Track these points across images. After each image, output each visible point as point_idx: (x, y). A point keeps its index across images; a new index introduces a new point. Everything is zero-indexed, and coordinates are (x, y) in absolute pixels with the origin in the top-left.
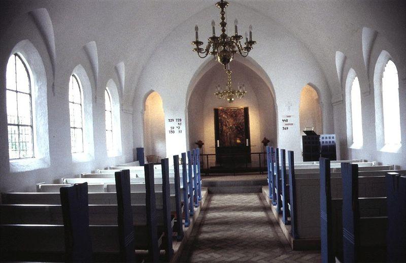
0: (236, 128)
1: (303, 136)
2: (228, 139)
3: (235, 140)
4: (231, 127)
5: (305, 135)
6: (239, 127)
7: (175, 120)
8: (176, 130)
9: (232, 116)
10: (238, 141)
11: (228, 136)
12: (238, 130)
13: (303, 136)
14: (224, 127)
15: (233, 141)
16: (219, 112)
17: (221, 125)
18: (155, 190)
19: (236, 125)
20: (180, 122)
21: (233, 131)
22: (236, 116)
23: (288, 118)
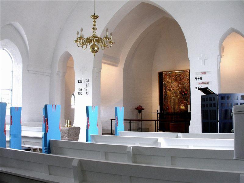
0: (181, 92)
1: (202, 96)
2: (172, 105)
3: (179, 106)
4: (175, 93)
5: (204, 94)
6: (183, 92)
7: (83, 81)
8: (84, 91)
9: (176, 80)
10: (182, 107)
11: (172, 101)
12: (182, 94)
13: (202, 96)
14: (168, 92)
15: (177, 107)
16: (164, 76)
17: (165, 90)
18: (23, 128)
19: (180, 90)
20: (87, 83)
21: (177, 96)
22: (181, 80)
23: (203, 76)
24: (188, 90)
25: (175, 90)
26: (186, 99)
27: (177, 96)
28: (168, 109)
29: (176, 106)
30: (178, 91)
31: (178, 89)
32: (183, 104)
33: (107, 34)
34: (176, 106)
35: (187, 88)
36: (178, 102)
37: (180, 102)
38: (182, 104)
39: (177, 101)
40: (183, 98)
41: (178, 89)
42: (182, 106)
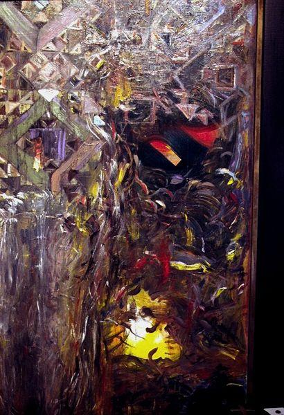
3: (102, 316)
12: (152, 160)
15: (63, 330)
21: (76, 181)
24: (232, 109)
25: (49, 94)
26: (199, 218)
27: (76, 181)
28: (185, 387)
29: (57, 323)
30: (85, 97)
31: (95, 83)
32: (159, 304)
33: (225, 353)
34: (57, 323)
35: (225, 76)
36: (89, 263)
37: (115, 264)
38: (143, 299)
39: (66, 256)
40: (162, 217)
41: (95, 83)
42: (140, 325)
